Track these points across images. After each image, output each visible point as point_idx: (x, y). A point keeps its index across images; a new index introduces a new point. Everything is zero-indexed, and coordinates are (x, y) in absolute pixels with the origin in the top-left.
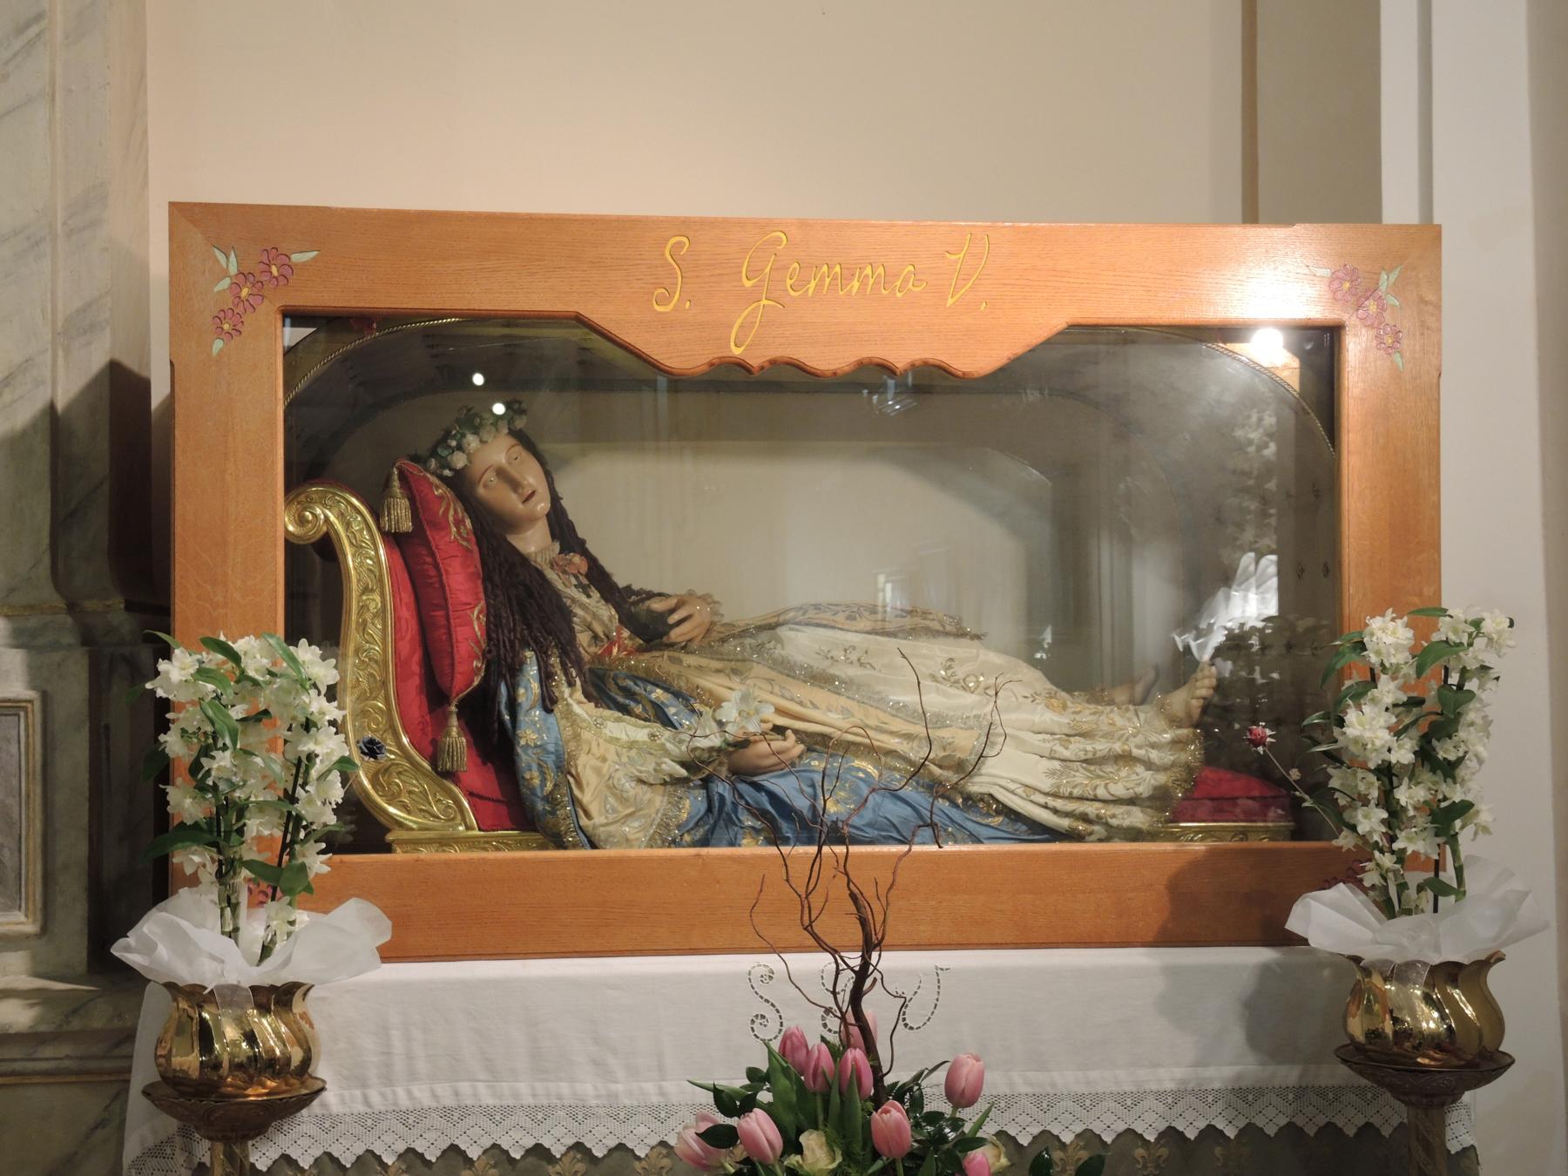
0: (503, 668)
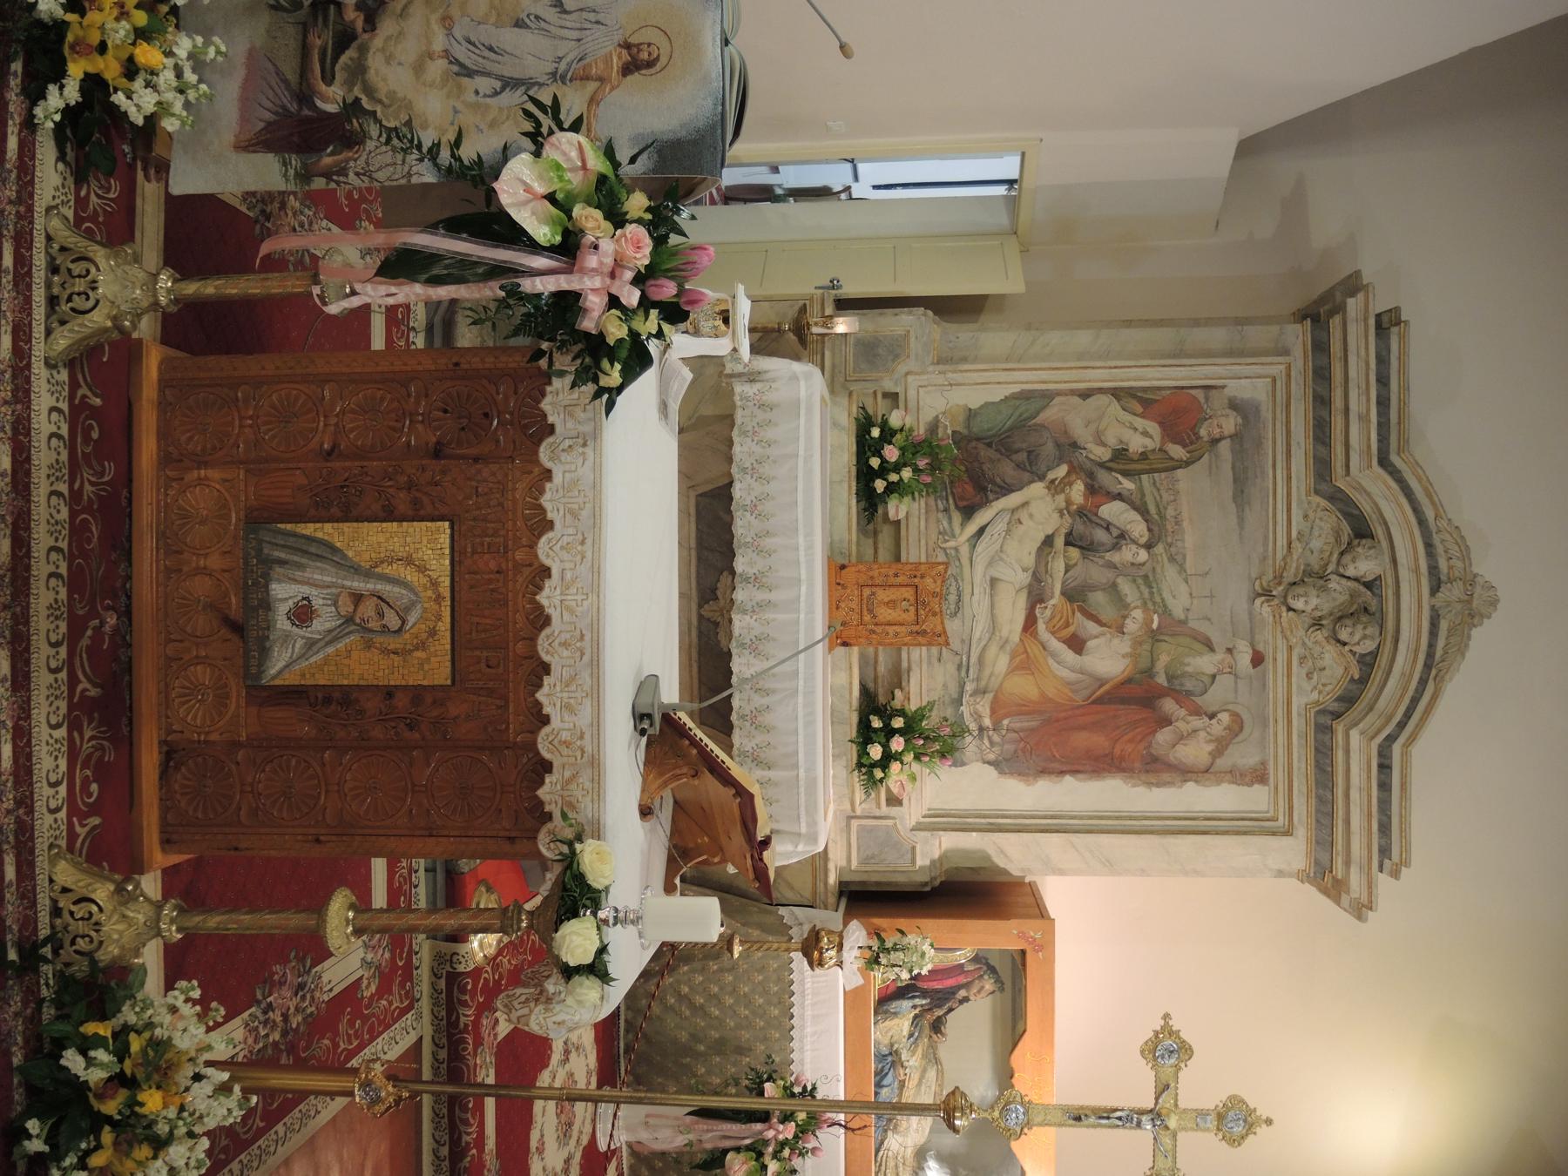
0: (924, 994)
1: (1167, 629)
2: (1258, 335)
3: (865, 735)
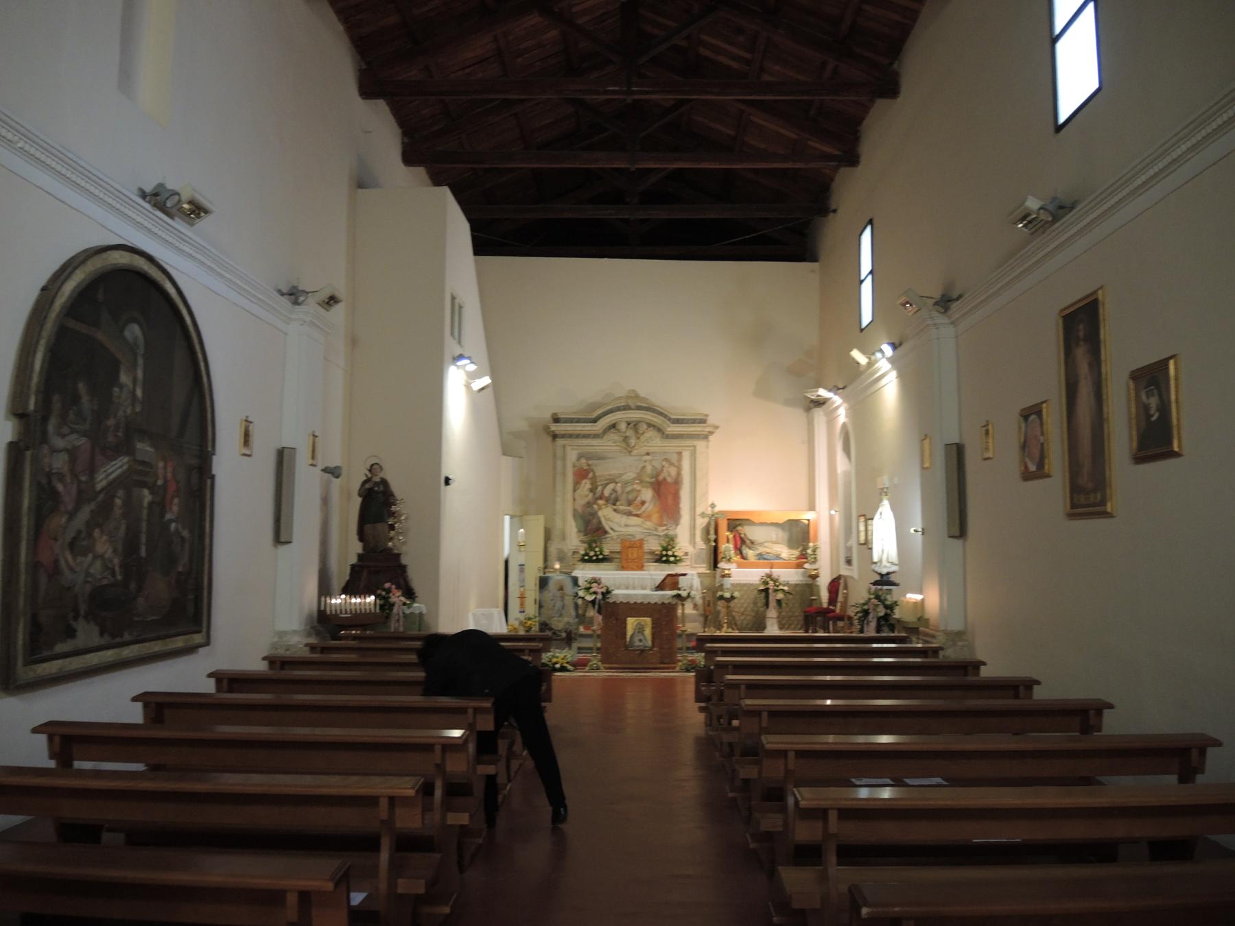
1: (639, 478)
2: (559, 453)
3: (667, 562)
